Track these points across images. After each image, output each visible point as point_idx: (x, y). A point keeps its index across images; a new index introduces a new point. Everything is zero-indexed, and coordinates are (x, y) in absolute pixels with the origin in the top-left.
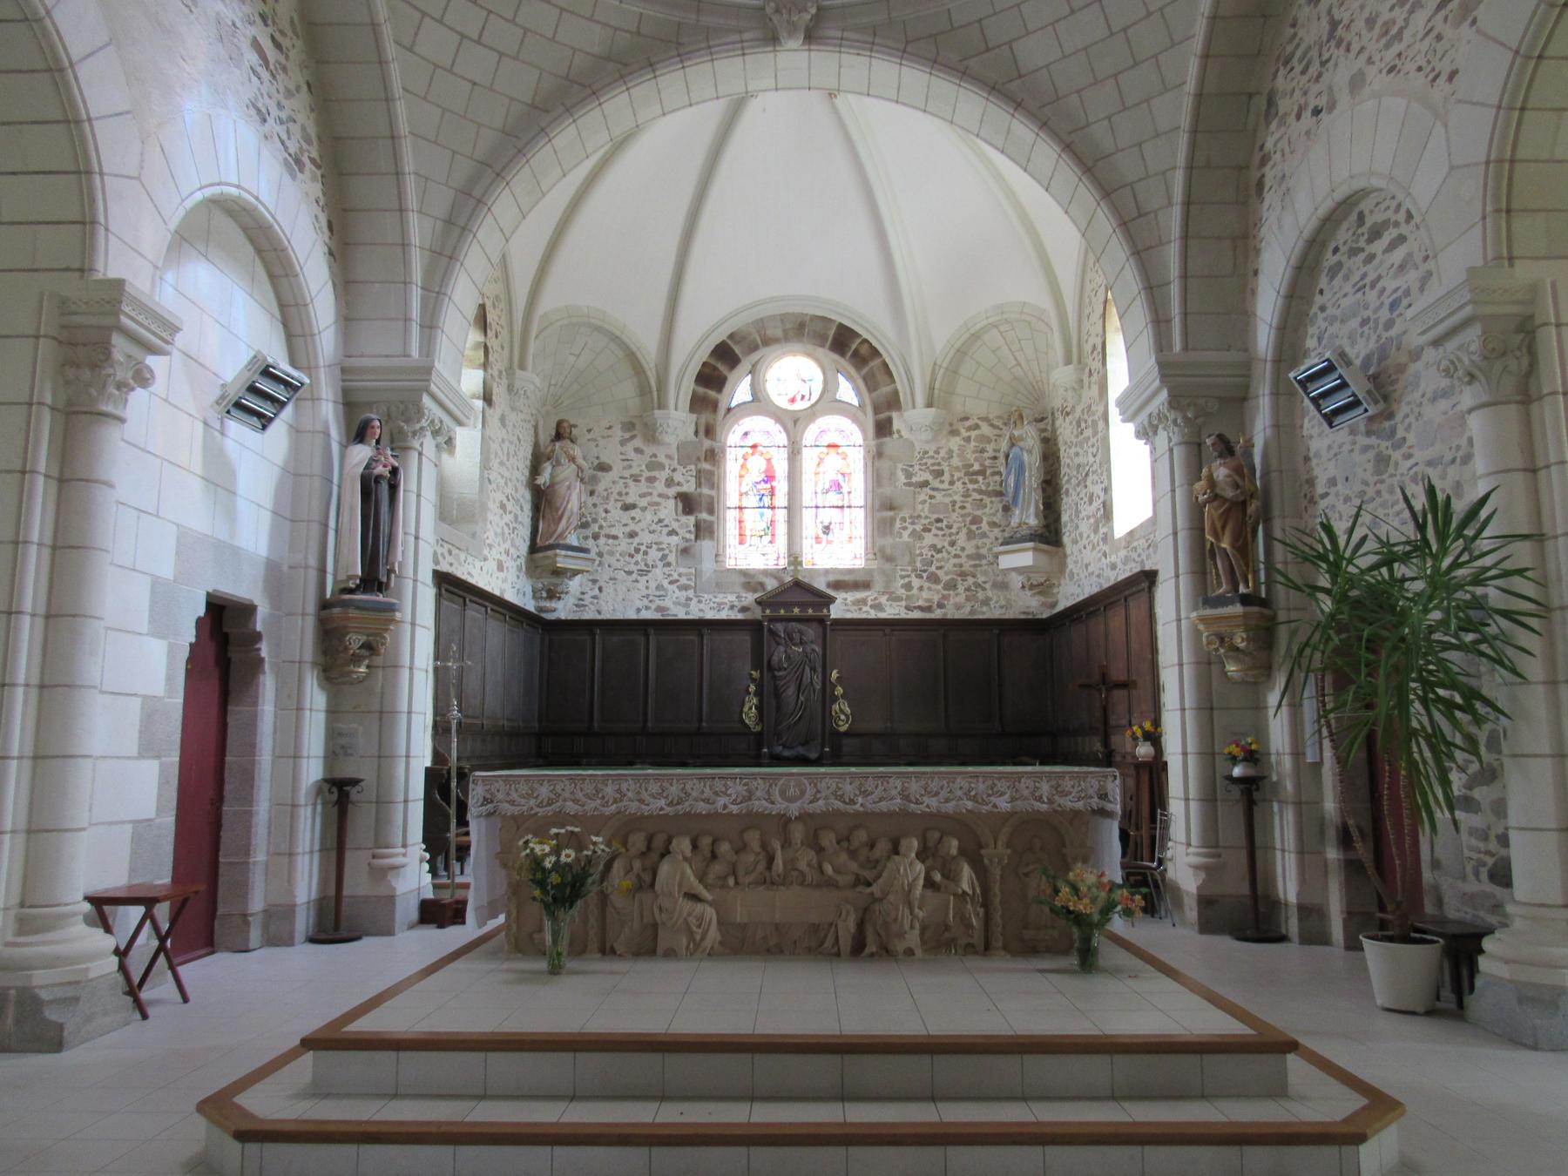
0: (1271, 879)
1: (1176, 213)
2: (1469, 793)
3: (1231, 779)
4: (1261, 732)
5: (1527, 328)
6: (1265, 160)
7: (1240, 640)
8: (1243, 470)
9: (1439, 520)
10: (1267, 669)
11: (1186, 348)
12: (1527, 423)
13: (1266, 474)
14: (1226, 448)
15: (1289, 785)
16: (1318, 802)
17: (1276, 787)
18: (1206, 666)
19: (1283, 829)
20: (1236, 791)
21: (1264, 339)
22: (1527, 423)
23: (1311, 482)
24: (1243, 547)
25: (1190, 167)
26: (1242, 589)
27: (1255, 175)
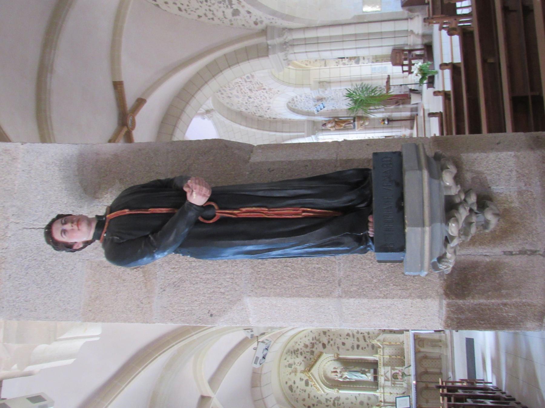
0: (407, 117)
1: (278, 134)
2: (410, 14)
3: (388, 124)
4: (379, 119)
5: (320, 82)
6: (270, 118)
7: (362, 122)
8: (329, 122)
9: (350, 95)
10: (367, 118)
11: (304, 132)
12: (334, 82)
13: (330, 118)
14: (324, 125)
15: (389, 114)
16: (392, 109)
17: (389, 116)
18: (366, 128)
19: (396, 115)
20: (390, 123)
21: (304, 118)
22: (334, 82)
23: (332, 110)
24: (344, 122)
25: (270, 131)
26: (352, 122)
27: (272, 119)
